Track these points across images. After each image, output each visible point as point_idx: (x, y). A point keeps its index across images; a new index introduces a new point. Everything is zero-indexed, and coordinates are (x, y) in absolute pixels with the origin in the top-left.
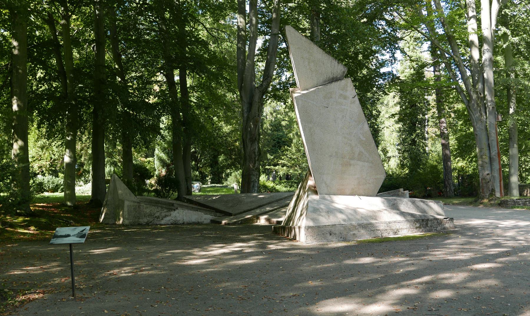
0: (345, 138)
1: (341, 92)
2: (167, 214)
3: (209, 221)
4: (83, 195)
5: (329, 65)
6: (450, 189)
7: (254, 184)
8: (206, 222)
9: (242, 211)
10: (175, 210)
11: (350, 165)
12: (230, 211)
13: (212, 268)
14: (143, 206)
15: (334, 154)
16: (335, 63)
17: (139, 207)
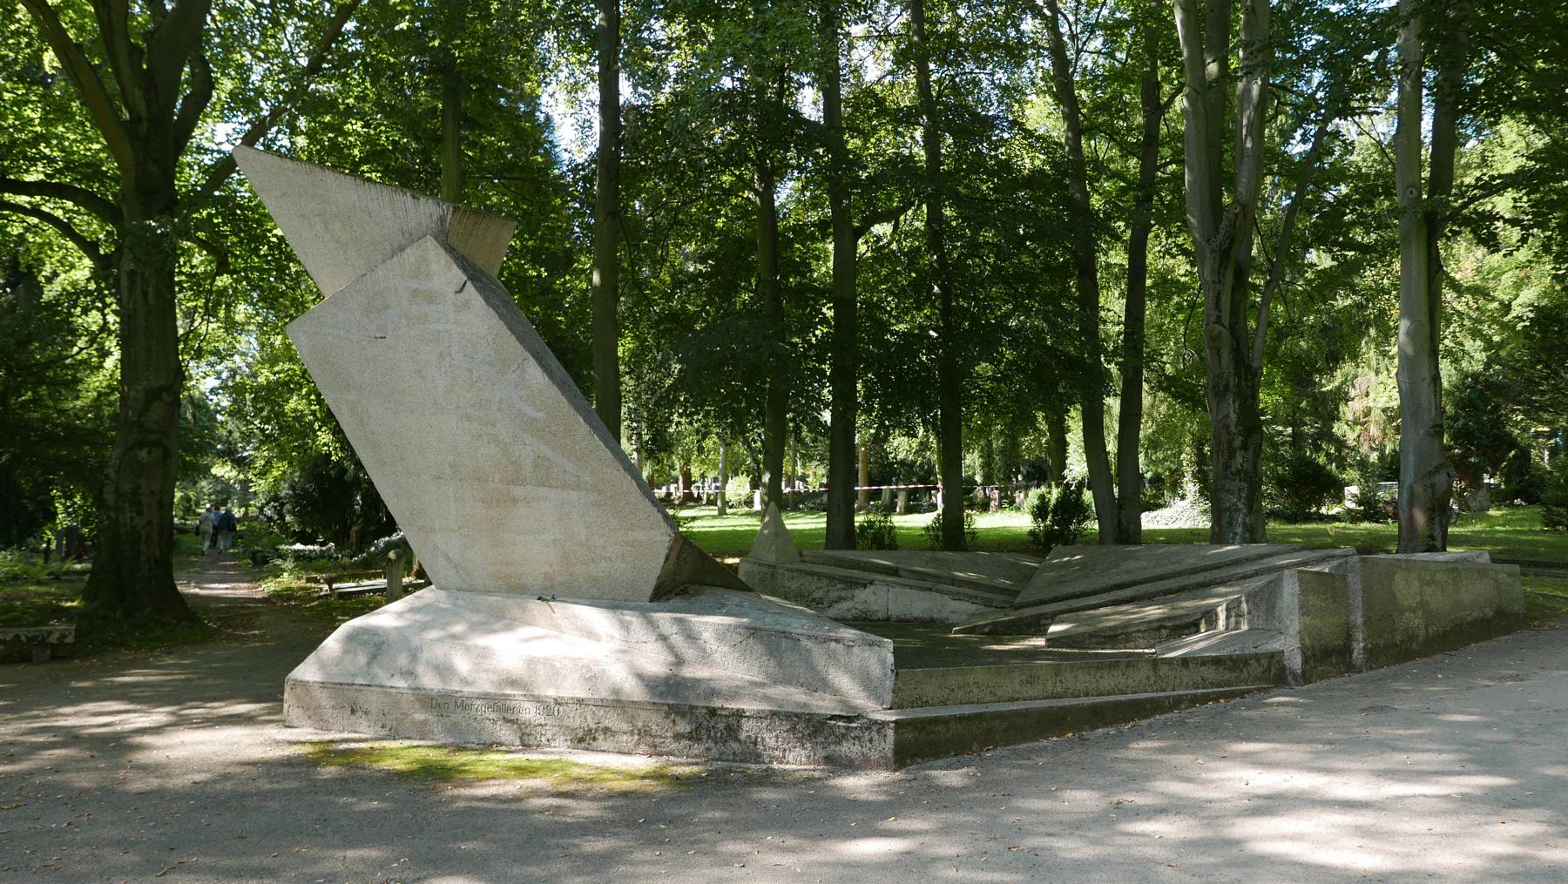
0: (468, 418)
1: (414, 284)
2: (844, 594)
4: (1175, 526)
7: (1231, 518)
10: (865, 586)
11: (514, 501)
15: (448, 471)
16: (405, 200)
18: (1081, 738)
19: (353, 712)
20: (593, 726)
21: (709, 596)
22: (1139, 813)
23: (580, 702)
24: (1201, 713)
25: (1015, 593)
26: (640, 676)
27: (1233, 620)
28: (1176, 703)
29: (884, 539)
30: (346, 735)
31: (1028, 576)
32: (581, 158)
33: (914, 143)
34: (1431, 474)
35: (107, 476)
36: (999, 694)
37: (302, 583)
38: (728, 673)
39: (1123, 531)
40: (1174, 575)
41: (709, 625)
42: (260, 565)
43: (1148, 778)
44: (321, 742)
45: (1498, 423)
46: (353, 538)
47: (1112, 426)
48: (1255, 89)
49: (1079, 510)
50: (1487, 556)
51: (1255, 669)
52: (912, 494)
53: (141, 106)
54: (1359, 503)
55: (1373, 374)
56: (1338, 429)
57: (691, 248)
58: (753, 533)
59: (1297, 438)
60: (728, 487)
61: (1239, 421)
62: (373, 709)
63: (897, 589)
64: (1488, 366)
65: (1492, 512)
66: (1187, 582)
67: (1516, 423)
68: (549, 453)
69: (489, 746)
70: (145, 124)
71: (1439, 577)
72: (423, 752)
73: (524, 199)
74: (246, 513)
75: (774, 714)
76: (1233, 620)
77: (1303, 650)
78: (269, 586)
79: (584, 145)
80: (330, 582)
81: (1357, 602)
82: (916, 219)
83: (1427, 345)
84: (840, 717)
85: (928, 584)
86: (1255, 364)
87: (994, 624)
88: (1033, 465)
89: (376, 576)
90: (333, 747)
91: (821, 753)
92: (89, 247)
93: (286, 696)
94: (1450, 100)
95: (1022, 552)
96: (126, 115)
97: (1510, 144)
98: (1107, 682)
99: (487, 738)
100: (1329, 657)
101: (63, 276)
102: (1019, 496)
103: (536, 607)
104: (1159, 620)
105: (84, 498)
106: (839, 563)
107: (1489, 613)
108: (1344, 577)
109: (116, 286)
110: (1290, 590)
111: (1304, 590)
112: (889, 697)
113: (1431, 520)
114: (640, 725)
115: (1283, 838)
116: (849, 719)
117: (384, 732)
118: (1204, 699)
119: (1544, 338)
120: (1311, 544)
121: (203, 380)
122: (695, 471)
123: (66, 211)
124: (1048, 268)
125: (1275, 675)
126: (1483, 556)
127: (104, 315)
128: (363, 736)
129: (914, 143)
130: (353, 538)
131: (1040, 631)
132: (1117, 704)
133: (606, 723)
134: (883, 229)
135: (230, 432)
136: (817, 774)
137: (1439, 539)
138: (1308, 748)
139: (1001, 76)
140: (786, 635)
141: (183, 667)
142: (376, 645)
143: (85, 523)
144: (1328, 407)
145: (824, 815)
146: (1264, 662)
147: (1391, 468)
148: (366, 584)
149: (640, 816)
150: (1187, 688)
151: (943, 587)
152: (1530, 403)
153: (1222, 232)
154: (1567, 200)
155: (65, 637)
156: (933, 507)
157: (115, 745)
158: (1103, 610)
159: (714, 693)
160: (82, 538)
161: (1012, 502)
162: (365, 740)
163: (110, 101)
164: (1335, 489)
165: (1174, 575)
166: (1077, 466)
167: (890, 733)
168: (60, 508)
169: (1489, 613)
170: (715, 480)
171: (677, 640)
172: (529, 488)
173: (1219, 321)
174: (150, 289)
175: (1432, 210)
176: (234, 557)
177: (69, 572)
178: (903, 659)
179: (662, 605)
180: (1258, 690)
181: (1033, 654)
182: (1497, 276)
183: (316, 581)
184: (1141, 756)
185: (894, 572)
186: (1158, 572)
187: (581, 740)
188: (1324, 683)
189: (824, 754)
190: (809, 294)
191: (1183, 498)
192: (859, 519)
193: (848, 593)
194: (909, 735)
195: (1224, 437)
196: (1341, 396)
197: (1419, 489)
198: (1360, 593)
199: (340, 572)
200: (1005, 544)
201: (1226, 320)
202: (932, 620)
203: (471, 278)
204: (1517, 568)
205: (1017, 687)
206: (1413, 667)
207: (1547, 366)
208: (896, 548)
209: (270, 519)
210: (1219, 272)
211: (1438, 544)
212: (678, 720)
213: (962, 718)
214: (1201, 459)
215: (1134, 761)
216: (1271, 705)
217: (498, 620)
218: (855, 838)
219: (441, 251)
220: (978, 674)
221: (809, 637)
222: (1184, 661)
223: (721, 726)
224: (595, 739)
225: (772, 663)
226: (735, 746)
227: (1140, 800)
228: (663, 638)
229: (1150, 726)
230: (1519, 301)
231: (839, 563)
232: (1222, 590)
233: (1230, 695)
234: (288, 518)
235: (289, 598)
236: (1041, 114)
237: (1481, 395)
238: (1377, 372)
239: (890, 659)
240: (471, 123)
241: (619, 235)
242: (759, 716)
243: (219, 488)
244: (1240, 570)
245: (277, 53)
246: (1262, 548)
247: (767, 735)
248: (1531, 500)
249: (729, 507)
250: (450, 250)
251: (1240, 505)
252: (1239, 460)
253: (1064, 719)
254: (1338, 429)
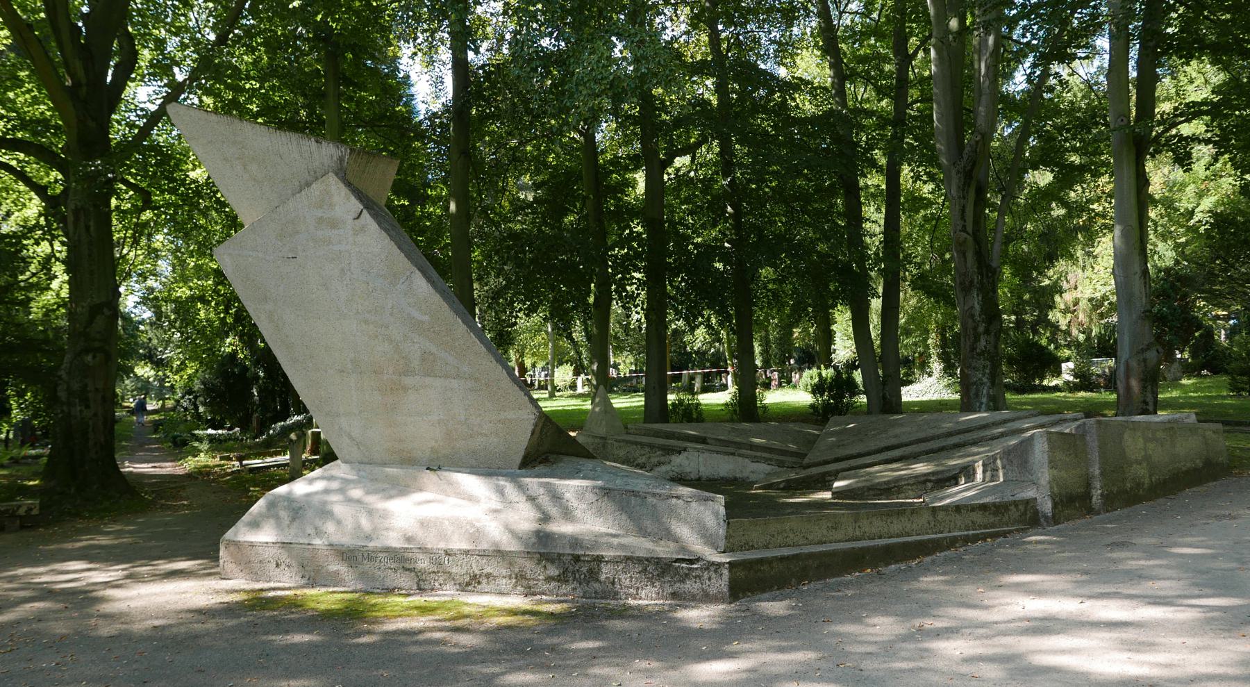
0: (366, 322)
1: (319, 213)
2: (662, 459)
4: (925, 398)
7: (977, 390)
10: (680, 453)
13: (1190, 546)
15: (349, 366)
16: (308, 145)
17: (604, 446)
18: (879, 573)
20: (477, 572)
21: (569, 463)
22: (938, 634)
23: (466, 552)
24: (969, 553)
25: (803, 456)
26: (513, 533)
27: (988, 474)
28: (953, 543)
29: (692, 414)
30: (272, 585)
31: (811, 441)
32: (436, 107)
33: (706, 88)
34: (1143, 351)
35: (60, 377)
36: (811, 538)
37: (217, 461)
38: (588, 526)
39: (887, 402)
40: (933, 438)
41: (571, 487)
42: (180, 446)
43: (939, 604)
44: (253, 591)
45: (1187, 308)
46: (255, 423)
47: (875, 320)
48: (991, 40)
49: (851, 387)
50: (1194, 417)
51: (1014, 513)
52: (706, 377)
53: (81, 73)
54: (1076, 376)
55: (1080, 271)
56: (1054, 316)
57: (526, 179)
58: (585, 412)
59: (1020, 324)
60: (556, 374)
61: (983, 311)
63: (707, 455)
64: (1177, 262)
65: (1184, 381)
66: (944, 444)
67: (1200, 308)
68: (434, 349)
69: (390, 591)
70: (84, 89)
71: (1159, 434)
72: (339, 596)
73: (392, 143)
74: (163, 405)
75: (628, 558)
76: (988, 474)
77: (1053, 497)
78: (190, 464)
79: (437, 97)
80: (240, 459)
81: (1095, 456)
82: (710, 152)
83: (1137, 245)
84: (683, 560)
85: (731, 450)
86: (994, 264)
87: (788, 481)
88: (800, 350)
89: (277, 453)
90: (264, 594)
92: (41, 190)
93: (221, 553)
94: (1151, 44)
95: (803, 421)
96: (69, 83)
97: (1198, 80)
98: (896, 527)
99: (389, 584)
100: (1073, 504)
101: (16, 214)
102: (795, 377)
103: (429, 478)
104: (925, 475)
105: (35, 396)
106: (657, 434)
107: (1199, 463)
108: (1083, 436)
109: (63, 219)
110: (1040, 451)
111: (1052, 448)
112: (722, 544)
113: (1144, 388)
114: (517, 570)
115: (1063, 652)
116: (691, 562)
117: (303, 582)
118: (975, 539)
119: (1222, 238)
120: (1043, 410)
121: (130, 301)
122: (528, 362)
123: (19, 161)
124: (819, 189)
125: (1030, 518)
126: (1190, 416)
127: (52, 245)
128: (287, 585)
129: (706, 88)
130: (255, 423)
131: (826, 486)
132: (920, 543)
133: (488, 570)
134: (682, 161)
135: (150, 339)
136: (666, 608)
137: (1151, 403)
138: (1068, 578)
139: (775, 34)
140: (635, 493)
141: (130, 532)
142: (297, 510)
143: (35, 416)
144: (1045, 299)
145: (683, 645)
146: (1021, 507)
147: (1105, 347)
148: (270, 460)
149: (515, 644)
150: (960, 530)
151: (744, 451)
152: (1211, 292)
153: (965, 157)
154: (1245, 125)
155: (31, 509)
156: (724, 387)
157: (83, 599)
158: (877, 468)
159: (596, 544)
160: (33, 429)
161: (789, 382)
162: (289, 589)
163: (55, 69)
164: (1053, 365)
165: (933, 438)
166: (844, 349)
167: (726, 572)
168: (14, 405)
169: (1199, 463)
170: (543, 369)
171: (545, 500)
172: (417, 378)
173: (964, 229)
174: (92, 223)
175: (1141, 139)
176: (157, 441)
177: (25, 457)
178: (734, 510)
179: (530, 471)
180: (1017, 530)
181: (822, 505)
182: (1194, 187)
183: (229, 459)
184: (931, 587)
185: (703, 440)
186: (921, 435)
187: (468, 584)
188: (1070, 524)
189: (671, 590)
190: (626, 213)
191: (930, 376)
192: (671, 398)
193: (667, 459)
194: (741, 574)
195: (970, 324)
196: (1056, 289)
197: (1134, 364)
198: (1097, 449)
199: (246, 451)
200: (789, 415)
201: (970, 228)
202: (736, 479)
203: (366, 207)
204: (1220, 426)
205: (825, 532)
206: (1142, 509)
207: (1225, 261)
208: (703, 421)
209: (186, 409)
210: (964, 189)
211: (1151, 408)
212: (549, 565)
213: (782, 559)
214: (944, 343)
215: (926, 591)
216: (1030, 543)
217: (401, 489)
218: (708, 659)
219: (341, 185)
220: (793, 522)
221: (654, 495)
222: (958, 508)
223: (584, 569)
224: (479, 583)
225: (624, 517)
226: (597, 585)
227: (938, 624)
228: (532, 499)
229: (933, 562)
230: (1200, 208)
231: (657, 434)
232: (975, 449)
233: (994, 536)
234: (201, 409)
235: (208, 474)
236: (810, 65)
237: (1174, 286)
238: (1084, 268)
239: (722, 510)
240: (348, 82)
241: (469, 171)
242: (615, 561)
243: (139, 385)
244: (988, 433)
245: (187, 29)
246: (1005, 414)
247: (622, 576)
248: (1215, 371)
249: (566, 390)
250: (348, 184)
251: (985, 380)
252: (983, 343)
253: (864, 557)
254: (1054, 316)
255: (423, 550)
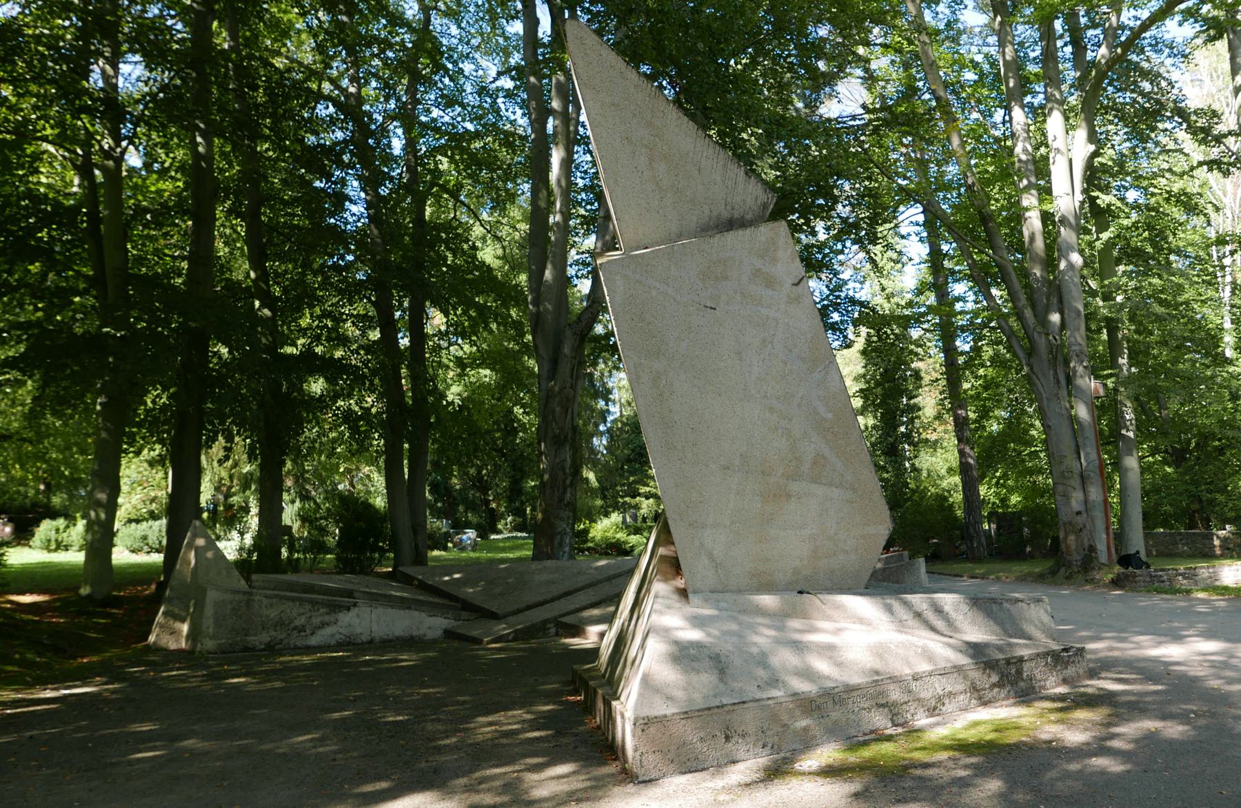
0: (771, 410)
1: (758, 263)
2: (327, 618)
3: (439, 633)
5: (718, 179)
6: (979, 542)
7: (562, 540)
8: (431, 635)
9: (523, 605)
10: (348, 609)
11: (789, 496)
12: (493, 606)
14: (260, 601)
15: (737, 462)
19: (727, 738)
20: (941, 693)
62: (751, 729)
91: (1061, 677)
133: (949, 688)
140: (994, 600)
202: (412, 637)
255: (894, 679)
